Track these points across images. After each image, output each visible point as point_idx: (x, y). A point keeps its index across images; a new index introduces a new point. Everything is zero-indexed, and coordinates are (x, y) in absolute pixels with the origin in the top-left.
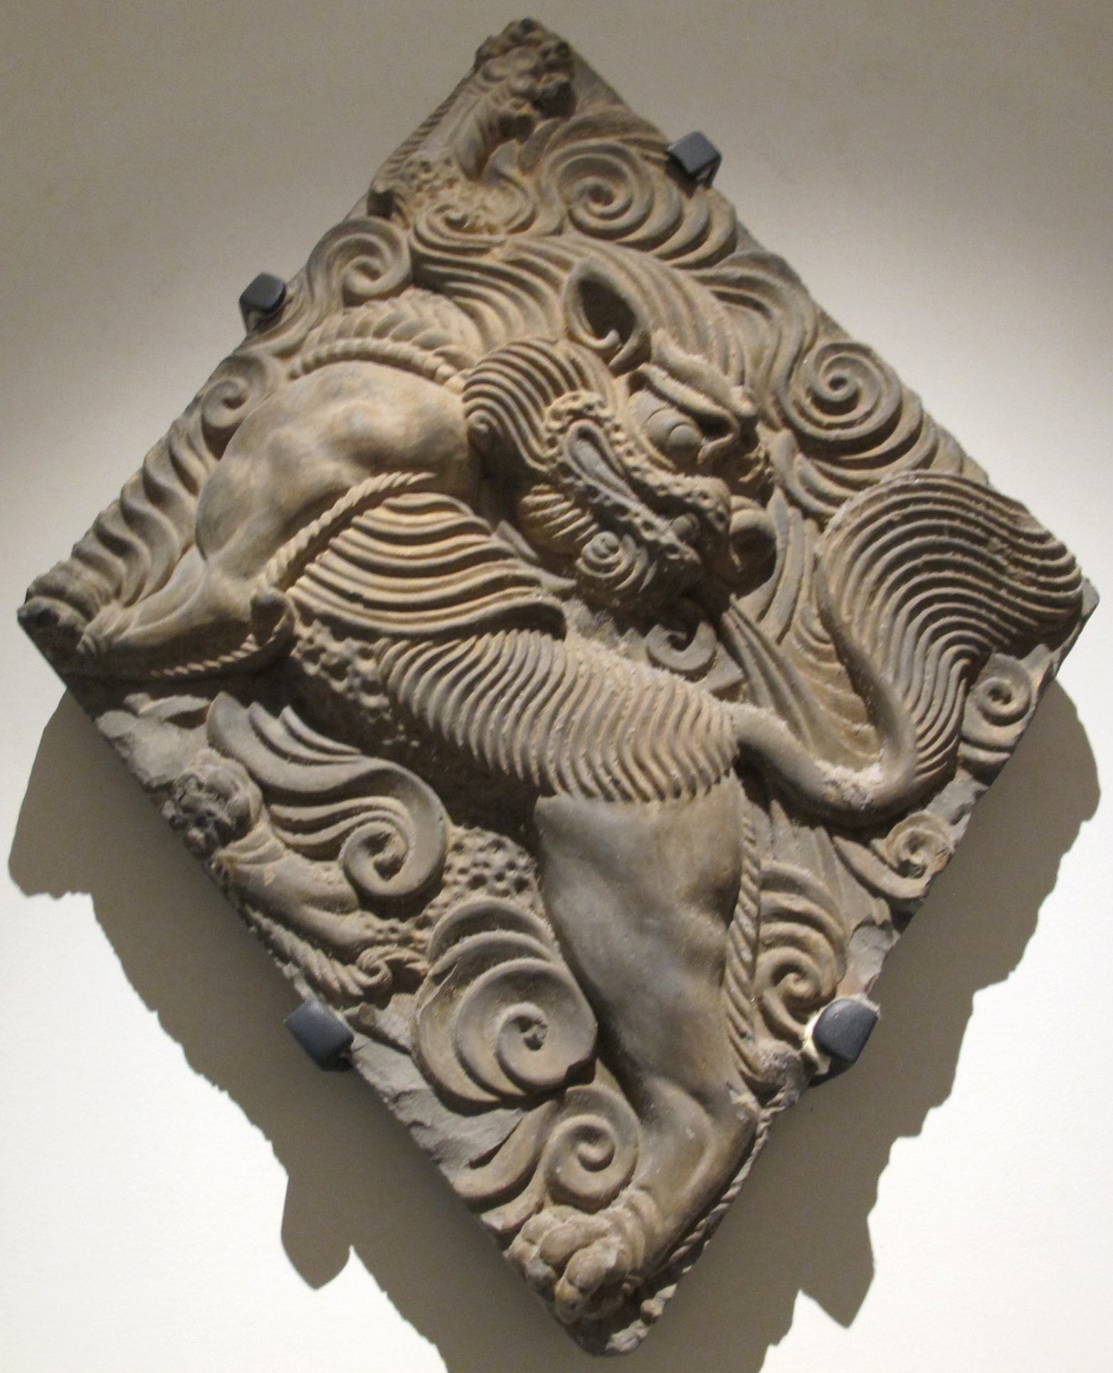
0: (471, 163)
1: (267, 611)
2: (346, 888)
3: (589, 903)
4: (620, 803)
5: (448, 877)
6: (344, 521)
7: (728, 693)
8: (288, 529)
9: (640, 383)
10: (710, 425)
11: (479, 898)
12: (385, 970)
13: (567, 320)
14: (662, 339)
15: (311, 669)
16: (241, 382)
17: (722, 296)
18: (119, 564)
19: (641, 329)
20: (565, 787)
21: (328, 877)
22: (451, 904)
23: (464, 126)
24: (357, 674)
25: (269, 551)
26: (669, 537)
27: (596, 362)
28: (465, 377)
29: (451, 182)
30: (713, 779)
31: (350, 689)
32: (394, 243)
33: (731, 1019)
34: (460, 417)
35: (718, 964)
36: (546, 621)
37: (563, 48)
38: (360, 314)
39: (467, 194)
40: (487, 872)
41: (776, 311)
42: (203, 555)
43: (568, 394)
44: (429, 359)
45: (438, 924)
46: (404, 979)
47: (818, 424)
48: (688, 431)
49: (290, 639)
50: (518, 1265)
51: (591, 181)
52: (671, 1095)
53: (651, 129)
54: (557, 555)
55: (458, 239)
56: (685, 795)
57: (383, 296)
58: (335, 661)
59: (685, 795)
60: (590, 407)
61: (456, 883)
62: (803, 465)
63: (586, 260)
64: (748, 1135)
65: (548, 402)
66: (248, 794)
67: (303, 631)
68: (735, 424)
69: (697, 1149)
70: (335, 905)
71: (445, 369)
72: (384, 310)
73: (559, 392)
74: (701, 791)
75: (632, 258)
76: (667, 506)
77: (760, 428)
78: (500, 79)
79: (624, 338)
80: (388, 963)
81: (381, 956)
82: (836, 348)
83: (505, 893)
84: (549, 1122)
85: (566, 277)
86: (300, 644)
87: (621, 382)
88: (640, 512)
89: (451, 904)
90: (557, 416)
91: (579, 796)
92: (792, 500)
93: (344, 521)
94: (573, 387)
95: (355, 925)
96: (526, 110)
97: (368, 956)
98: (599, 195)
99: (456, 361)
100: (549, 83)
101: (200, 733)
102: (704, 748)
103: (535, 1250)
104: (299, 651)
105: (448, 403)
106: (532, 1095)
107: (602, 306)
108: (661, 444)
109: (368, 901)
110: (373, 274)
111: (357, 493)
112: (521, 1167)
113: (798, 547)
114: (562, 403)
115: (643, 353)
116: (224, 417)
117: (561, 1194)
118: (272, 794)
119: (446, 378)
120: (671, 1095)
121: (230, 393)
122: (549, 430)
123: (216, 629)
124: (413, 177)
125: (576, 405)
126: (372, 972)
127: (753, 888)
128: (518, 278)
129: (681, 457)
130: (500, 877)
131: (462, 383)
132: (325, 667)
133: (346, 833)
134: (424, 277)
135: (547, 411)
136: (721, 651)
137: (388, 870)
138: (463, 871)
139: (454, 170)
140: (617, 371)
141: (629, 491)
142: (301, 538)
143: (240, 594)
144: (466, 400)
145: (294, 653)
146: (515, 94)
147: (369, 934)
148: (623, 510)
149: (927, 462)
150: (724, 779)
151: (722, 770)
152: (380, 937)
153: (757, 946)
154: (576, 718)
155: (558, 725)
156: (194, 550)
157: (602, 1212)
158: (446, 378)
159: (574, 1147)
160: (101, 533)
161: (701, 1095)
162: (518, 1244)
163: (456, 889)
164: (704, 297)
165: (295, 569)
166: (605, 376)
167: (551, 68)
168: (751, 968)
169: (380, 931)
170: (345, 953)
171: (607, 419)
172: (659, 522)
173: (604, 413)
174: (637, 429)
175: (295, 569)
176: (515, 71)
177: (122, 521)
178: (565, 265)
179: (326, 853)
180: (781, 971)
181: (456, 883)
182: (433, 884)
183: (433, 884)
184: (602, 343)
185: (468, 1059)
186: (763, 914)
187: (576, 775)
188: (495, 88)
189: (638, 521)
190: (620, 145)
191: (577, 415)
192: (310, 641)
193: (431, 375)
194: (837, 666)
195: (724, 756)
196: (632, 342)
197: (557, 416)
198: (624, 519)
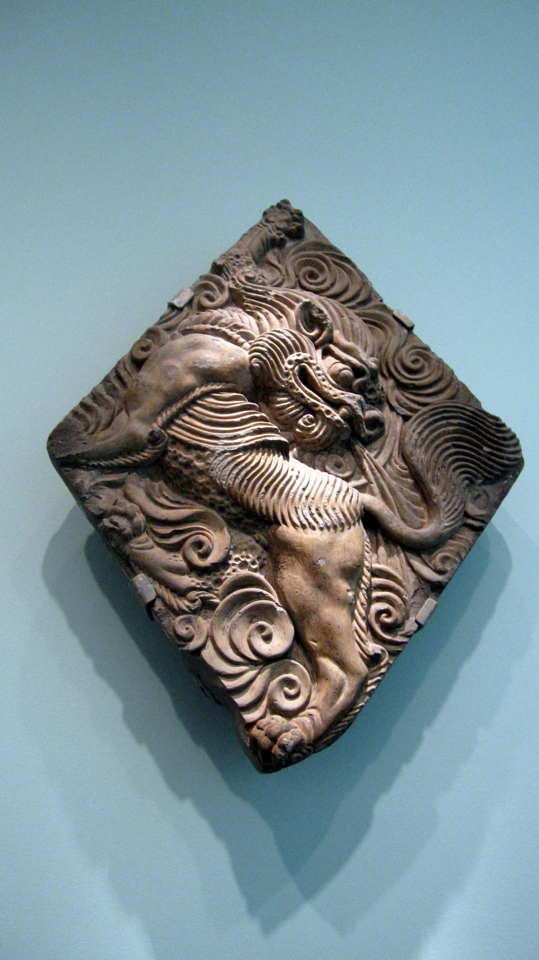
0: (257, 256)
1: (154, 439)
2: (183, 564)
3: (294, 578)
4: (309, 530)
5: (231, 562)
6: (194, 402)
7: (361, 488)
8: (169, 404)
9: (327, 353)
10: (358, 372)
11: (245, 572)
12: (198, 602)
13: (297, 322)
14: (337, 334)
15: (174, 465)
16: (149, 341)
17: (365, 321)
18: (89, 417)
19: (320, 275)
20: (285, 523)
21: (178, 560)
22: (231, 574)
23: (256, 243)
24: (195, 467)
25: (159, 413)
26: (337, 417)
27: (310, 342)
28: (250, 344)
29: (248, 263)
30: (352, 522)
31: (192, 474)
32: (222, 288)
33: (356, 631)
34: (248, 360)
35: (351, 606)
36: (282, 449)
37: (300, 214)
38: (206, 314)
39: (256, 269)
40: (248, 560)
41: (390, 332)
42: (127, 412)
43: (296, 353)
44: (235, 335)
45: (225, 583)
46: (207, 606)
47: (406, 378)
48: (348, 372)
49: (165, 452)
50: (255, 741)
51: (309, 268)
52: (329, 665)
53: (339, 251)
54: (288, 424)
55: (250, 286)
56: (339, 529)
57: (215, 308)
58: (185, 461)
59: (339, 529)
60: (306, 359)
61: (234, 564)
62: (397, 392)
63: (307, 300)
64: (363, 684)
65: (286, 357)
66: (140, 518)
67: (171, 449)
68: (368, 371)
69: (339, 690)
70: (179, 571)
71: (242, 340)
72: (217, 313)
73: (291, 352)
74: (346, 527)
75: (327, 301)
76: (337, 405)
77: (380, 377)
78: (273, 222)
79: (322, 331)
80: (201, 598)
81: (197, 595)
82: (415, 347)
83: (255, 570)
84: (272, 676)
85: (298, 305)
86: (170, 454)
87: (319, 352)
88: (324, 407)
89: (231, 574)
90: (290, 363)
91: (291, 527)
92: (392, 408)
93: (194, 402)
94: (298, 350)
95: (186, 581)
96: (283, 236)
97: (193, 594)
98: (312, 275)
99: (248, 336)
100: (293, 227)
101: (120, 491)
102: (348, 509)
103: (263, 733)
104: (169, 457)
105: (242, 354)
106: (265, 661)
107: (311, 319)
108: (335, 376)
109: (193, 569)
110: (212, 299)
111: (198, 392)
112: (258, 694)
113: (393, 423)
114: (293, 357)
115: (330, 340)
116: (142, 355)
117: (274, 709)
118: (151, 519)
119: (242, 343)
120: (329, 665)
121: (144, 345)
122: (286, 369)
123: (133, 446)
124: (232, 259)
125: (300, 358)
126: (193, 601)
127: (368, 574)
128: (278, 306)
129: (344, 383)
130: (253, 563)
131: (249, 346)
132: (181, 464)
133: (185, 540)
134: (236, 299)
135: (286, 361)
136: (358, 470)
137: (204, 556)
138: (237, 559)
139: (250, 258)
140: (317, 347)
141: (322, 401)
142: (174, 409)
143: (142, 430)
144: (249, 354)
145: (167, 459)
146: (278, 229)
147: (193, 584)
148: (316, 405)
149: (452, 398)
150: (357, 524)
151: (356, 519)
152: (198, 586)
153: (370, 601)
154: (293, 490)
155: (284, 496)
156: (123, 413)
157: (294, 719)
158: (242, 343)
159: (282, 688)
160: (83, 405)
161: (342, 664)
162: (255, 731)
163: (234, 567)
164: (358, 323)
165: (170, 422)
166: (313, 348)
167: (296, 220)
168: (367, 611)
169: (198, 584)
170: (181, 593)
171: (314, 364)
172: (333, 412)
173: (312, 361)
174: (326, 371)
175: (170, 422)
176: (280, 220)
177: (124, 498)
178: (298, 300)
179: (176, 548)
180: (379, 613)
181: (234, 564)
182: (224, 564)
183: (224, 564)
184: (313, 334)
185: (237, 645)
186: (373, 585)
187: (291, 519)
188: (270, 226)
189: (323, 410)
190: (324, 255)
191: (298, 362)
192: (175, 452)
193: (236, 342)
194: (410, 480)
195: (357, 514)
196: (325, 333)
197: (290, 363)
198: (317, 409)
